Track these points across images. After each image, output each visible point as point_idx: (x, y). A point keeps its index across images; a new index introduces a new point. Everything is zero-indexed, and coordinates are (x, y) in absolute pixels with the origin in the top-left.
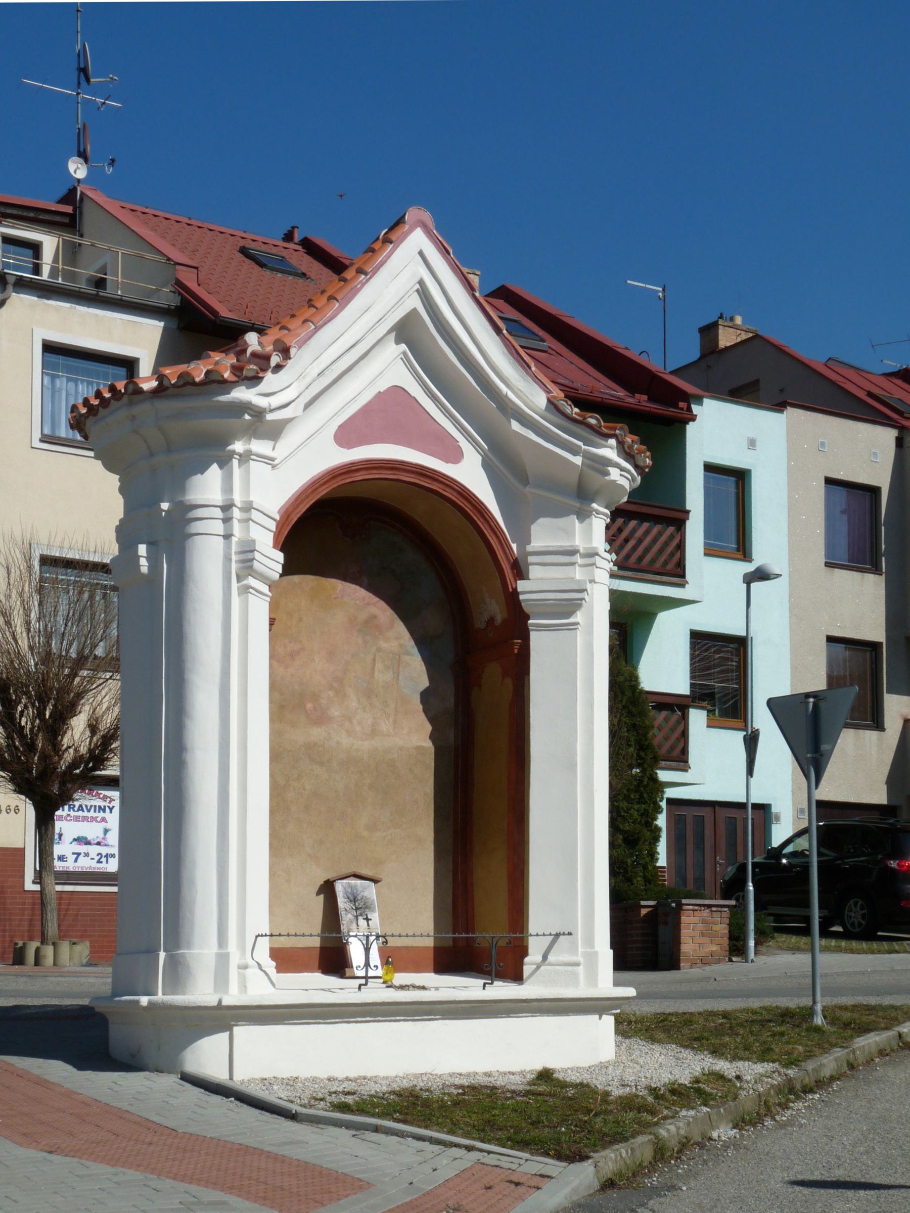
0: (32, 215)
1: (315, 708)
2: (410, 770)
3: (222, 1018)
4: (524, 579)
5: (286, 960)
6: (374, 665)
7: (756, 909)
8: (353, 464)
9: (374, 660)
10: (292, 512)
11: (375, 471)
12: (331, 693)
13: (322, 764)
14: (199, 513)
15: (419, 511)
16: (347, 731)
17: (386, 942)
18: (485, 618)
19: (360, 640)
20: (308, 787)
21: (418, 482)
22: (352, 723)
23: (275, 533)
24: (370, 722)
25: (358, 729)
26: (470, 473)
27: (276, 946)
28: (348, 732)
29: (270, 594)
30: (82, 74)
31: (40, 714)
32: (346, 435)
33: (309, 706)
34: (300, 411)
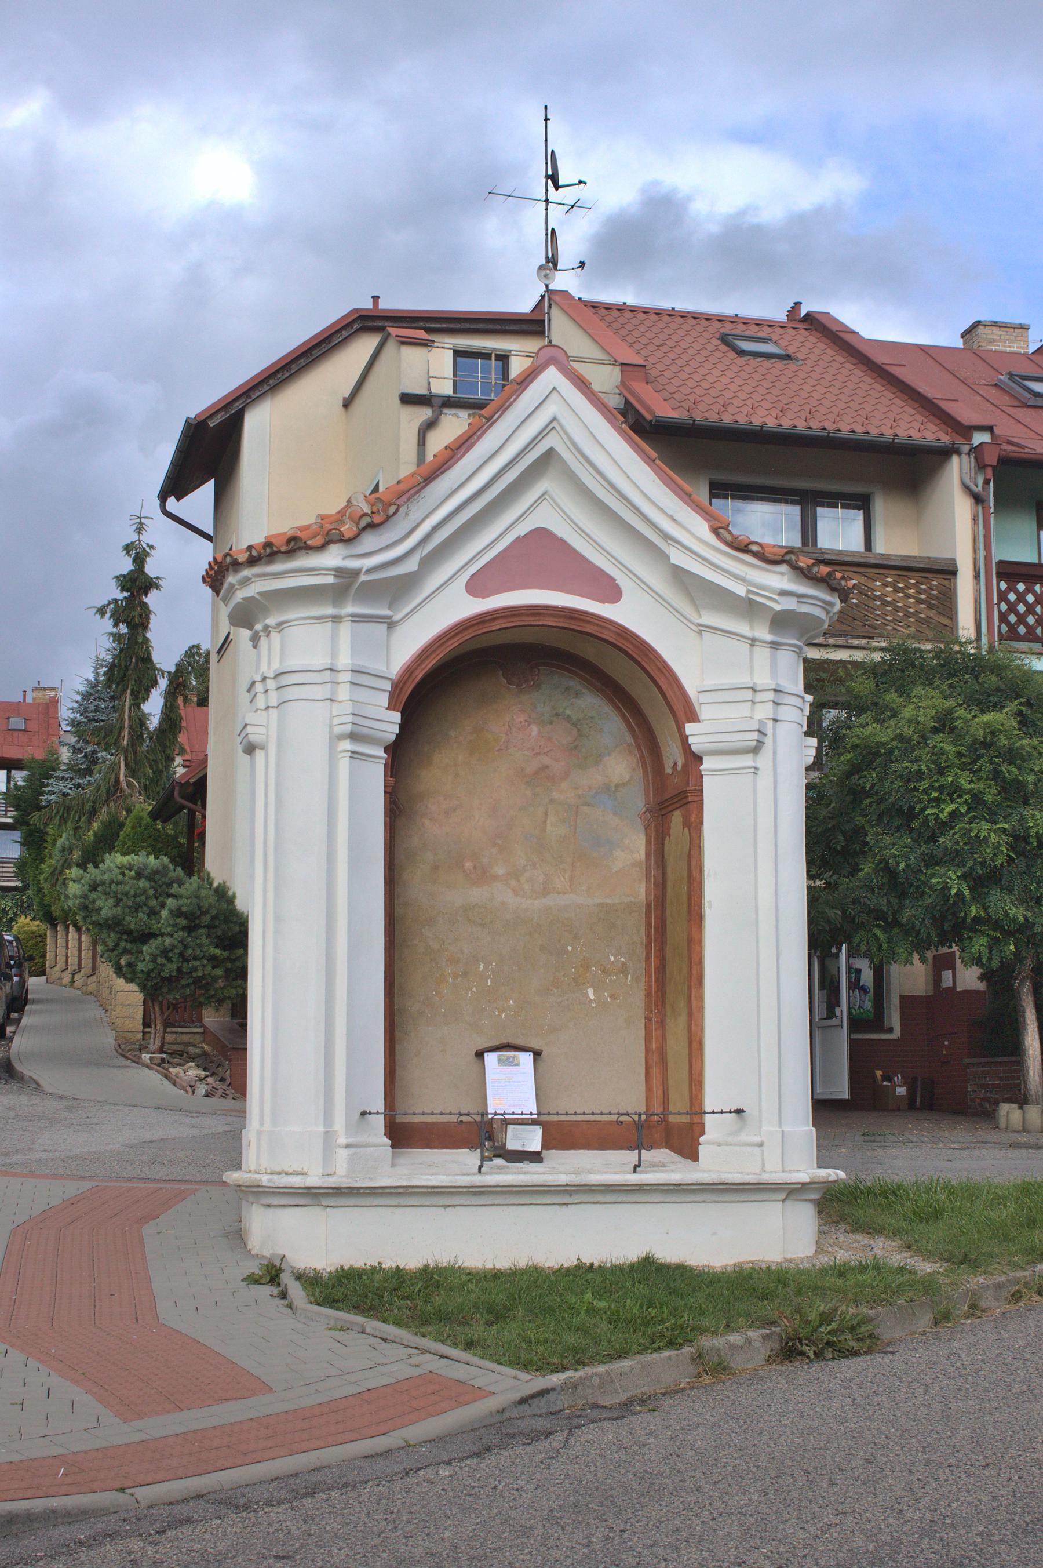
0: (410, 1190)
1: (475, 867)
6: (546, 818)
8: (487, 613)
9: (546, 814)
10: (416, 668)
12: (494, 851)
13: (483, 926)
14: (76, 705)
15: (588, 652)
19: (529, 793)
21: (566, 625)
22: (518, 881)
24: (541, 879)
26: (638, 612)
28: (516, 892)
29: (385, 756)
30: (550, 181)
31: (986, 820)
32: (476, 586)
33: (468, 865)
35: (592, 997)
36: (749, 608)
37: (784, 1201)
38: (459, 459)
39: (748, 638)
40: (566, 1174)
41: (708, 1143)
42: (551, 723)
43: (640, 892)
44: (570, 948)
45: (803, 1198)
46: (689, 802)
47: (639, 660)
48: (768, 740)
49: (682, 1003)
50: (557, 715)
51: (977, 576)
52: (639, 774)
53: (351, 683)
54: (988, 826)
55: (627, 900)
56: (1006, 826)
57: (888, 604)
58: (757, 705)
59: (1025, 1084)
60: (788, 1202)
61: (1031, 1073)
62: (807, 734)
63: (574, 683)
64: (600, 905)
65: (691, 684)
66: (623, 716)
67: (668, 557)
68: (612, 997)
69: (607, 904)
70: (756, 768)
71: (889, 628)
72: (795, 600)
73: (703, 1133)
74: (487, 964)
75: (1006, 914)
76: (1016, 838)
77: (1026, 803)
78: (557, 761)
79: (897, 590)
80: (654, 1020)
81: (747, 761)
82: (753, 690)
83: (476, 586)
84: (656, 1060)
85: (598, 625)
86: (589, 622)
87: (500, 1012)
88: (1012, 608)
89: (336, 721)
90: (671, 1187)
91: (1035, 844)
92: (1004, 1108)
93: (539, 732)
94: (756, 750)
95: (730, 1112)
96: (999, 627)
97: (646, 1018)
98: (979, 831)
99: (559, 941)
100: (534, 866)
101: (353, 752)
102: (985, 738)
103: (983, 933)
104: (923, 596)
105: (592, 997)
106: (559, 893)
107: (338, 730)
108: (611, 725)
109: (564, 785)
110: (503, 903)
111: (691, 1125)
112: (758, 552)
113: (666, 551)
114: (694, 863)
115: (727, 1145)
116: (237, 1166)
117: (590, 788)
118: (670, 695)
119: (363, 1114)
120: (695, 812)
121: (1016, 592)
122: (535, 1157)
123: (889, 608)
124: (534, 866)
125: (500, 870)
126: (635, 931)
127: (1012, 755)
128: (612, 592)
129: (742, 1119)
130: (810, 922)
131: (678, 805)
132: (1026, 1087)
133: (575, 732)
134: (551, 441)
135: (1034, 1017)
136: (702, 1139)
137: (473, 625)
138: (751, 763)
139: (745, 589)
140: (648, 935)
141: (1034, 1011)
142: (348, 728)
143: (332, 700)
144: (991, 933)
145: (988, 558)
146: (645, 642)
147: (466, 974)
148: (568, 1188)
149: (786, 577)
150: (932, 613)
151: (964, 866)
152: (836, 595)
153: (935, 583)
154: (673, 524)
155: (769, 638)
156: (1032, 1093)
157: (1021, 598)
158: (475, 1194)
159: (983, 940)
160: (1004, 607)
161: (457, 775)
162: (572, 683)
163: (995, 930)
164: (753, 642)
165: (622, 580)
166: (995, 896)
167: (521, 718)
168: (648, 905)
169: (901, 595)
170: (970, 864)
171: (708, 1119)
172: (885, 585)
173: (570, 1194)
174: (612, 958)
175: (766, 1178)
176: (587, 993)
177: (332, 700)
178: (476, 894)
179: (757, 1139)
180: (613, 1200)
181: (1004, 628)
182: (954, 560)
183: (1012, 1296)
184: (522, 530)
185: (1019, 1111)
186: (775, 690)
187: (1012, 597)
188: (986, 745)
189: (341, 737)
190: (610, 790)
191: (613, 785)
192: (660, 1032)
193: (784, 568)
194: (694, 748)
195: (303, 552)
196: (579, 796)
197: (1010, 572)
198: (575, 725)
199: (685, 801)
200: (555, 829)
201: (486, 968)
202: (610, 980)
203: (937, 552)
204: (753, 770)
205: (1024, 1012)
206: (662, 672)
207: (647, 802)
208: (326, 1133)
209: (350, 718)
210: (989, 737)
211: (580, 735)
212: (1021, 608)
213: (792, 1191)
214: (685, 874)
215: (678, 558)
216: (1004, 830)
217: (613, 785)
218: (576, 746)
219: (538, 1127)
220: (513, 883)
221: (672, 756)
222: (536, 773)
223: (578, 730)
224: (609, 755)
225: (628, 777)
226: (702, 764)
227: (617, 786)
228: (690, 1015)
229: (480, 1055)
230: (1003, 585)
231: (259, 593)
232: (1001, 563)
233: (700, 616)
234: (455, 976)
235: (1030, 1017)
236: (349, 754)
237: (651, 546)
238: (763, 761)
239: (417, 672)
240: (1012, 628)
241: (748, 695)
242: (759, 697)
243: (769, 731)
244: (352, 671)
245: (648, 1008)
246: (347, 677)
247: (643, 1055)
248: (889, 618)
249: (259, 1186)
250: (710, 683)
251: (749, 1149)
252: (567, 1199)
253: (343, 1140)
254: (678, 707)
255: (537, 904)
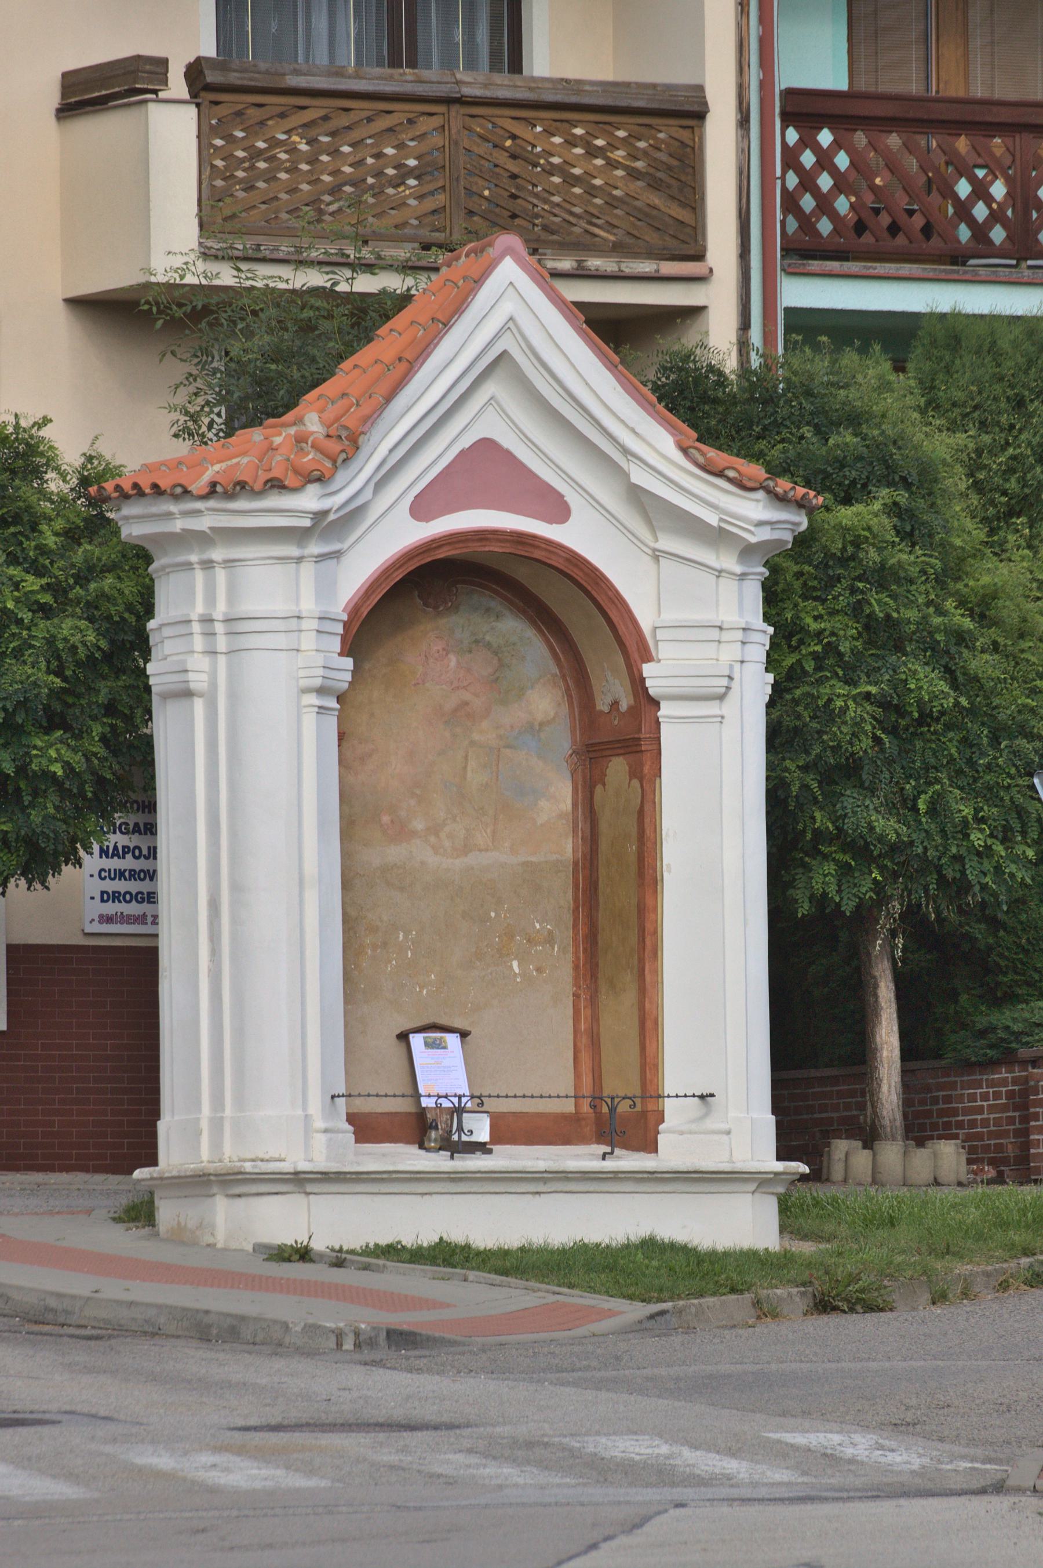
0: (394, 1176)
1: (392, 821)
2: (515, 892)
3: (233, 1182)
4: (649, 661)
5: (367, 1128)
6: (466, 763)
7: (908, 1053)
9: (466, 757)
11: (461, 545)
12: (413, 802)
13: (402, 889)
15: (522, 574)
16: (433, 847)
17: (482, 1104)
18: (609, 700)
19: (447, 734)
20: (385, 918)
22: (438, 837)
23: (352, 671)
25: (447, 844)
26: (582, 535)
27: (351, 1111)
28: (435, 850)
32: (422, 508)
33: (386, 819)
34: (368, 494)
35: (517, 971)
36: (717, 536)
37: (753, 1193)
38: (416, 372)
39: (716, 570)
40: (544, 1160)
41: (669, 1131)
42: (470, 652)
43: (566, 848)
44: (493, 914)
45: (771, 1190)
46: (642, 751)
47: (589, 588)
48: (735, 685)
49: (628, 978)
50: (477, 642)
51: (744, 122)
52: (565, 709)
53: (318, 631)
54: (842, 689)
55: (555, 857)
56: (874, 690)
57: (576, 180)
58: (722, 645)
59: (874, 1107)
60: (757, 1195)
61: (885, 1088)
62: (767, 670)
63: (495, 604)
64: (525, 864)
65: (645, 618)
66: (548, 642)
67: (627, 476)
68: (539, 970)
69: (532, 863)
70: (723, 717)
71: (577, 230)
72: (768, 528)
73: (662, 1120)
74: (407, 933)
75: (871, 828)
76: (884, 704)
77: (899, 648)
78: (477, 695)
79: (592, 152)
80: (583, 996)
81: (711, 708)
82: (721, 628)
83: (422, 508)
84: (589, 1043)
85: (546, 550)
86: (537, 547)
87: (422, 988)
88: (808, 182)
89: (302, 673)
90: (645, 1176)
91: (916, 715)
92: (841, 1147)
93: (458, 663)
94: (721, 698)
95: (694, 1096)
96: (783, 223)
97: (574, 995)
98: (830, 700)
99: (482, 905)
100: (454, 820)
101: (320, 707)
102: (844, 549)
103: (826, 857)
104: (639, 164)
105: (517, 971)
106: (480, 850)
107: (304, 683)
108: (532, 649)
109: (485, 724)
110: (422, 863)
111: (644, 1114)
112: (735, 478)
113: (625, 467)
114: (647, 820)
115: (690, 1133)
116: (153, 1161)
117: (512, 727)
118: (622, 629)
119: (333, 1097)
120: (649, 763)
121: (817, 148)
122: (482, 1148)
123: (577, 190)
124: (454, 820)
125: (419, 825)
126: (561, 894)
127: (884, 577)
128: (557, 509)
129: (707, 1105)
130: (152, 763)
131: (622, 751)
132: (875, 1113)
133: (495, 661)
134: (507, 343)
135: (891, 995)
136: (661, 1127)
137: (417, 555)
138: (718, 712)
139: (717, 518)
140: (576, 899)
141: (892, 986)
142: (318, 682)
143: (298, 650)
144: (839, 856)
145: (767, 84)
146: (597, 569)
147: (385, 944)
148: (545, 1175)
149: (761, 504)
150: (656, 200)
151: (807, 753)
152: (803, 512)
153: (661, 135)
154: (632, 436)
155: (738, 569)
156: (886, 1122)
157: (824, 161)
158: (453, 1180)
159: (830, 868)
160: (792, 180)
161: (372, 715)
162: (493, 604)
163: (844, 852)
164: (720, 573)
165: (571, 497)
166: (850, 799)
167: (438, 646)
168: (576, 864)
169: (599, 162)
170: (816, 750)
171: (670, 1106)
172: (571, 142)
173: (545, 1181)
174: (538, 926)
175: (739, 1166)
176: (511, 967)
177: (298, 650)
178: (395, 853)
179: (723, 1126)
180: (586, 1190)
181: (792, 225)
182: (700, 89)
183: (1000, 1285)
184: (466, 442)
185: (867, 1153)
186: (744, 629)
187: (808, 159)
188: (844, 561)
189: (306, 691)
190: (534, 729)
191: (536, 724)
192: (589, 1012)
193: (760, 495)
194: (651, 692)
195: (276, 491)
196: (500, 737)
197: (805, 109)
198: (496, 653)
199: (634, 749)
200: (476, 777)
201: (406, 937)
202: (536, 951)
203: (659, 70)
204: (719, 719)
205: (876, 986)
206: (613, 602)
207: (574, 742)
208: (306, 1116)
209: (320, 672)
210: (850, 549)
211: (502, 665)
212: (825, 182)
213: (762, 1181)
214: (634, 831)
215: (639, 477)
216: (868, 696)
217: (536, 724)
218: (497, 678)
219: (485, 1115)
220: (433, 839)
221: (611, 690)
222: (456, 710)
223: (500, 660)
224: (532, 687)
225: (552, 714)
226: (659, 709)
227: (541, 724)
228: (642, 991)
229: (403, 1037)
230: (792, 136)
231: (210, 528)
232: (790, 94)
233: (657, 540)
234: (374, 947)
235: (886, 993)
236: (316, 709)
237: (607, 460)
238: (728, 708)
239: (363, 609)
240: (807, 223)
241: (715, 634)
242: (726, 636)
243: (736, 676)
244: (320, 618)
245: (576, 983)
246: (314, 624)
247: (571, 1037)
248: (577, 210)
249: (241, 1173)
250: (669, 616)
251: (716, 1137)
252: (541, 1188)
253: (319, 1124)
254: (632, 647)
255: (459, 863)
